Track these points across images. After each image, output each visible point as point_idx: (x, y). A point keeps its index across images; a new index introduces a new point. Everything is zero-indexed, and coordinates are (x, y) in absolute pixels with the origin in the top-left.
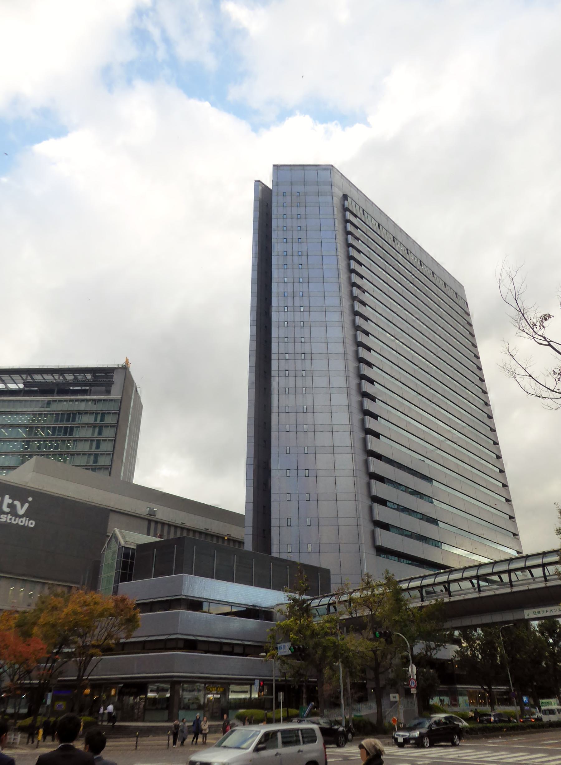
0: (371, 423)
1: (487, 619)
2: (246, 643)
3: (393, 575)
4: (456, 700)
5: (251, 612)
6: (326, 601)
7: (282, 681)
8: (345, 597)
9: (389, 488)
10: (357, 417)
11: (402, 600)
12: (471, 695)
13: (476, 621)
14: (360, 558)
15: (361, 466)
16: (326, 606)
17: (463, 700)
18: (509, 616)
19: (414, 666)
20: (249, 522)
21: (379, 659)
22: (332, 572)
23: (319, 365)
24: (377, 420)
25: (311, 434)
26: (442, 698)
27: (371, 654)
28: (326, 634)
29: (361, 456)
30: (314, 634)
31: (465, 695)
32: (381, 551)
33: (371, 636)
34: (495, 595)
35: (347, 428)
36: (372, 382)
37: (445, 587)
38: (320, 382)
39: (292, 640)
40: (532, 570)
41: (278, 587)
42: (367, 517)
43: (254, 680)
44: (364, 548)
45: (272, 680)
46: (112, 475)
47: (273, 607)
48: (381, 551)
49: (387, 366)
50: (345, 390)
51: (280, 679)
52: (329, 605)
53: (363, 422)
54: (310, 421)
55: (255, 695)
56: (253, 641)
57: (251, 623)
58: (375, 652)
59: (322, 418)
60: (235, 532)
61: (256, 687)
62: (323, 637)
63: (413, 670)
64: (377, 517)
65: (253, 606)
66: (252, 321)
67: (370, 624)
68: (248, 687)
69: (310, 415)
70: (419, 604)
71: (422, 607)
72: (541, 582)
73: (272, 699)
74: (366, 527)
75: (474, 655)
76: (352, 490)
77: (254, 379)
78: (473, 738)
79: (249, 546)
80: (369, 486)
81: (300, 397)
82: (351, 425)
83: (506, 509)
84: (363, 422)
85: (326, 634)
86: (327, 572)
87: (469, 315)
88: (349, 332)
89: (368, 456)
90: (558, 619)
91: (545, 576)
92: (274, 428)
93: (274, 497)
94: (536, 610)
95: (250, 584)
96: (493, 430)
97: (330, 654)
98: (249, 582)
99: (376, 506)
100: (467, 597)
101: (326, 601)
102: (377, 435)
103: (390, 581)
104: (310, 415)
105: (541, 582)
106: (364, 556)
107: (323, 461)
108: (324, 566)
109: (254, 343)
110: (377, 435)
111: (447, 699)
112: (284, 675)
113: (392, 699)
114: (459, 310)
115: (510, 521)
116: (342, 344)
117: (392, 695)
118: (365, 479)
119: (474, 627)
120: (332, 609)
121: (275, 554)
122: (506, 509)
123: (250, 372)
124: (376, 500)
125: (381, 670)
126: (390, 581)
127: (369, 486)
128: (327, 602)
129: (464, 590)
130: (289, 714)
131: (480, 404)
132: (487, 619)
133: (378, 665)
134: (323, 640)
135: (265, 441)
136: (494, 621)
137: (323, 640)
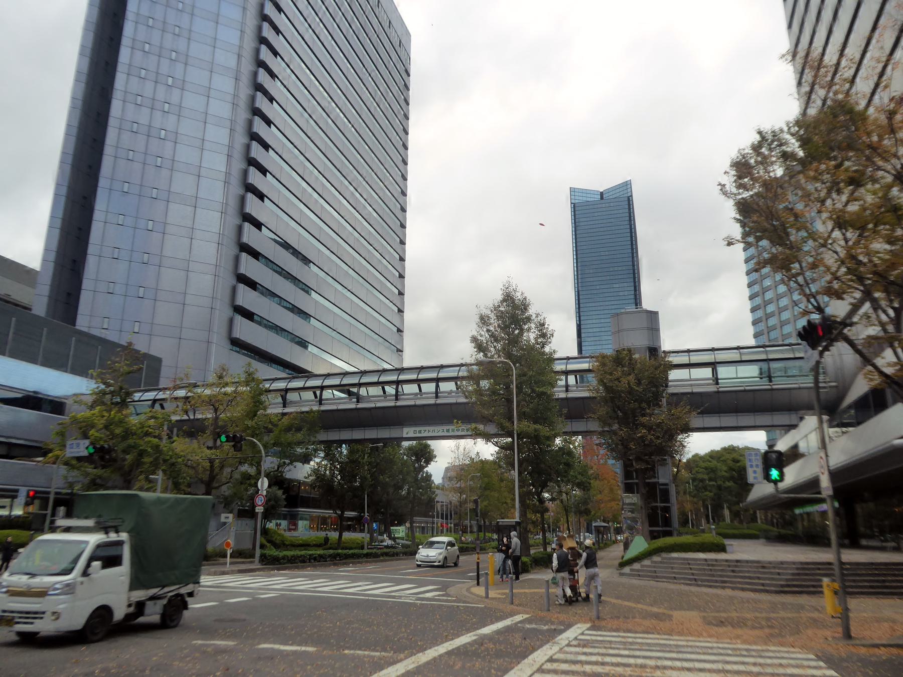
0: (255, 177)
1: (358, 434)
2: (14, 441)
3: (256, 370)
4: (296, 525)
5: (31, 401)
6: (151, 395)
7: (67, 494)
8: (181, 393)
9: (259, 272)
10: (239, 164)
11: (261, 403)
12: (312, 519)
13: (346, 435)
14: (208, 350)
15: (231, 233)
16: (150, 403)
17: (301, 524)
18: (384, 433)
19: (266, 480)
20: (44, 288)
21: (217, 470)
22: (163, 364)
23: (197, 76)
24: (265, 176)
25: (165, 173)
26: (279, 521)
27: (207, 464)
28: (147, 434)
29: (234, 220)
30: (128, 434)
31: (306, 519)
32: (237, 344)
33: (210, 444)
34: (376, 408)
35: (222, 177)
36: (264, 171)
37: (315, 393)
38: (193, 101)
39: (92, 438)
40: (422, 385)
41: (79, 370)
42: (227, 299)
43: (17, 491)
44: (215, 338)
45: (48, 493)
46: (43, 610)
47: (67, 397)
48: (237, 344)
49: (295, 110)
50: (228, 124)
51: (64, 491)
52: (155, 401)
53: (245, 173)
54: (168, 153)
55: (18, 512)
56: (26, 440)
57: (27, 415)
58: (212, 461)
59: (186, 154)
60: (18, 293)
61: (21, 499)
62: (141, 438)
63: (263, 484)
64: (239, 302)
65: (35, 392)
66: (78, 72)
67: (211, 428)
68: (8, 500)
69: (169, 145)
70: (280, 410)
71: (284, 414)
72: (431, 398)
73: (45, 515)
74: (224, 312)
75: (333, 475)
76: (214, 262)
77: (85, 69)
78: (321, 566)
79: (40, 308)
80: (237, 260)
81: (158, 114)
82: (228, 174)
83: (396, 320)
84: (245, 173)
85: (147, 434)
86: (159, 361)
87: (409, 75)
88: (249, 43)
89: (244, 221)
90: (429, 442)
91: (437, 393)
92: (113, 122)
93: (92, 249)
94: (418, 429)
95: (33, 360)
96: (403, 226)
97: (147, 460)
98: (32, 359)
99: (241, 287)
100: (341, 407)
101: (151, 395)
102: (261, 196)
103: (250, 379)
104: (169, 145)
105: (431, 398)
106: (214, 348)
107: (178, 213)
108: (153, 352)
109: (57, 233)
110: (261, 196)
111: (284, 523)
112: (71, 485)
113: (223, 520)
114: (400, 66)
115: (397, 335)
116: (236, 56)
117: (223, 516)
118: (234, 250)
119: (340, 443)
120: (157, 406)
121: (77, 327)
122: (396, 320)
123: (77, 80)
124: (243, 279)
125: (215, 485)
126: (250, 379)
127: (237, 260)
128: (152, 398)
129: (335, 399)
130: (822, 397)
131: (397, 191)
132: (358, 434)
133: (212, 478)
134: (141, 442)
135: (90, 167)
136: (367, 437)
137: (141, 442)
